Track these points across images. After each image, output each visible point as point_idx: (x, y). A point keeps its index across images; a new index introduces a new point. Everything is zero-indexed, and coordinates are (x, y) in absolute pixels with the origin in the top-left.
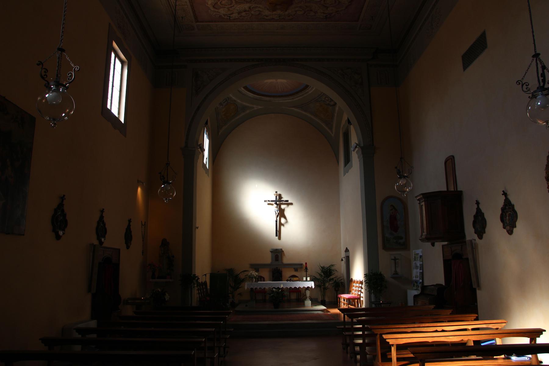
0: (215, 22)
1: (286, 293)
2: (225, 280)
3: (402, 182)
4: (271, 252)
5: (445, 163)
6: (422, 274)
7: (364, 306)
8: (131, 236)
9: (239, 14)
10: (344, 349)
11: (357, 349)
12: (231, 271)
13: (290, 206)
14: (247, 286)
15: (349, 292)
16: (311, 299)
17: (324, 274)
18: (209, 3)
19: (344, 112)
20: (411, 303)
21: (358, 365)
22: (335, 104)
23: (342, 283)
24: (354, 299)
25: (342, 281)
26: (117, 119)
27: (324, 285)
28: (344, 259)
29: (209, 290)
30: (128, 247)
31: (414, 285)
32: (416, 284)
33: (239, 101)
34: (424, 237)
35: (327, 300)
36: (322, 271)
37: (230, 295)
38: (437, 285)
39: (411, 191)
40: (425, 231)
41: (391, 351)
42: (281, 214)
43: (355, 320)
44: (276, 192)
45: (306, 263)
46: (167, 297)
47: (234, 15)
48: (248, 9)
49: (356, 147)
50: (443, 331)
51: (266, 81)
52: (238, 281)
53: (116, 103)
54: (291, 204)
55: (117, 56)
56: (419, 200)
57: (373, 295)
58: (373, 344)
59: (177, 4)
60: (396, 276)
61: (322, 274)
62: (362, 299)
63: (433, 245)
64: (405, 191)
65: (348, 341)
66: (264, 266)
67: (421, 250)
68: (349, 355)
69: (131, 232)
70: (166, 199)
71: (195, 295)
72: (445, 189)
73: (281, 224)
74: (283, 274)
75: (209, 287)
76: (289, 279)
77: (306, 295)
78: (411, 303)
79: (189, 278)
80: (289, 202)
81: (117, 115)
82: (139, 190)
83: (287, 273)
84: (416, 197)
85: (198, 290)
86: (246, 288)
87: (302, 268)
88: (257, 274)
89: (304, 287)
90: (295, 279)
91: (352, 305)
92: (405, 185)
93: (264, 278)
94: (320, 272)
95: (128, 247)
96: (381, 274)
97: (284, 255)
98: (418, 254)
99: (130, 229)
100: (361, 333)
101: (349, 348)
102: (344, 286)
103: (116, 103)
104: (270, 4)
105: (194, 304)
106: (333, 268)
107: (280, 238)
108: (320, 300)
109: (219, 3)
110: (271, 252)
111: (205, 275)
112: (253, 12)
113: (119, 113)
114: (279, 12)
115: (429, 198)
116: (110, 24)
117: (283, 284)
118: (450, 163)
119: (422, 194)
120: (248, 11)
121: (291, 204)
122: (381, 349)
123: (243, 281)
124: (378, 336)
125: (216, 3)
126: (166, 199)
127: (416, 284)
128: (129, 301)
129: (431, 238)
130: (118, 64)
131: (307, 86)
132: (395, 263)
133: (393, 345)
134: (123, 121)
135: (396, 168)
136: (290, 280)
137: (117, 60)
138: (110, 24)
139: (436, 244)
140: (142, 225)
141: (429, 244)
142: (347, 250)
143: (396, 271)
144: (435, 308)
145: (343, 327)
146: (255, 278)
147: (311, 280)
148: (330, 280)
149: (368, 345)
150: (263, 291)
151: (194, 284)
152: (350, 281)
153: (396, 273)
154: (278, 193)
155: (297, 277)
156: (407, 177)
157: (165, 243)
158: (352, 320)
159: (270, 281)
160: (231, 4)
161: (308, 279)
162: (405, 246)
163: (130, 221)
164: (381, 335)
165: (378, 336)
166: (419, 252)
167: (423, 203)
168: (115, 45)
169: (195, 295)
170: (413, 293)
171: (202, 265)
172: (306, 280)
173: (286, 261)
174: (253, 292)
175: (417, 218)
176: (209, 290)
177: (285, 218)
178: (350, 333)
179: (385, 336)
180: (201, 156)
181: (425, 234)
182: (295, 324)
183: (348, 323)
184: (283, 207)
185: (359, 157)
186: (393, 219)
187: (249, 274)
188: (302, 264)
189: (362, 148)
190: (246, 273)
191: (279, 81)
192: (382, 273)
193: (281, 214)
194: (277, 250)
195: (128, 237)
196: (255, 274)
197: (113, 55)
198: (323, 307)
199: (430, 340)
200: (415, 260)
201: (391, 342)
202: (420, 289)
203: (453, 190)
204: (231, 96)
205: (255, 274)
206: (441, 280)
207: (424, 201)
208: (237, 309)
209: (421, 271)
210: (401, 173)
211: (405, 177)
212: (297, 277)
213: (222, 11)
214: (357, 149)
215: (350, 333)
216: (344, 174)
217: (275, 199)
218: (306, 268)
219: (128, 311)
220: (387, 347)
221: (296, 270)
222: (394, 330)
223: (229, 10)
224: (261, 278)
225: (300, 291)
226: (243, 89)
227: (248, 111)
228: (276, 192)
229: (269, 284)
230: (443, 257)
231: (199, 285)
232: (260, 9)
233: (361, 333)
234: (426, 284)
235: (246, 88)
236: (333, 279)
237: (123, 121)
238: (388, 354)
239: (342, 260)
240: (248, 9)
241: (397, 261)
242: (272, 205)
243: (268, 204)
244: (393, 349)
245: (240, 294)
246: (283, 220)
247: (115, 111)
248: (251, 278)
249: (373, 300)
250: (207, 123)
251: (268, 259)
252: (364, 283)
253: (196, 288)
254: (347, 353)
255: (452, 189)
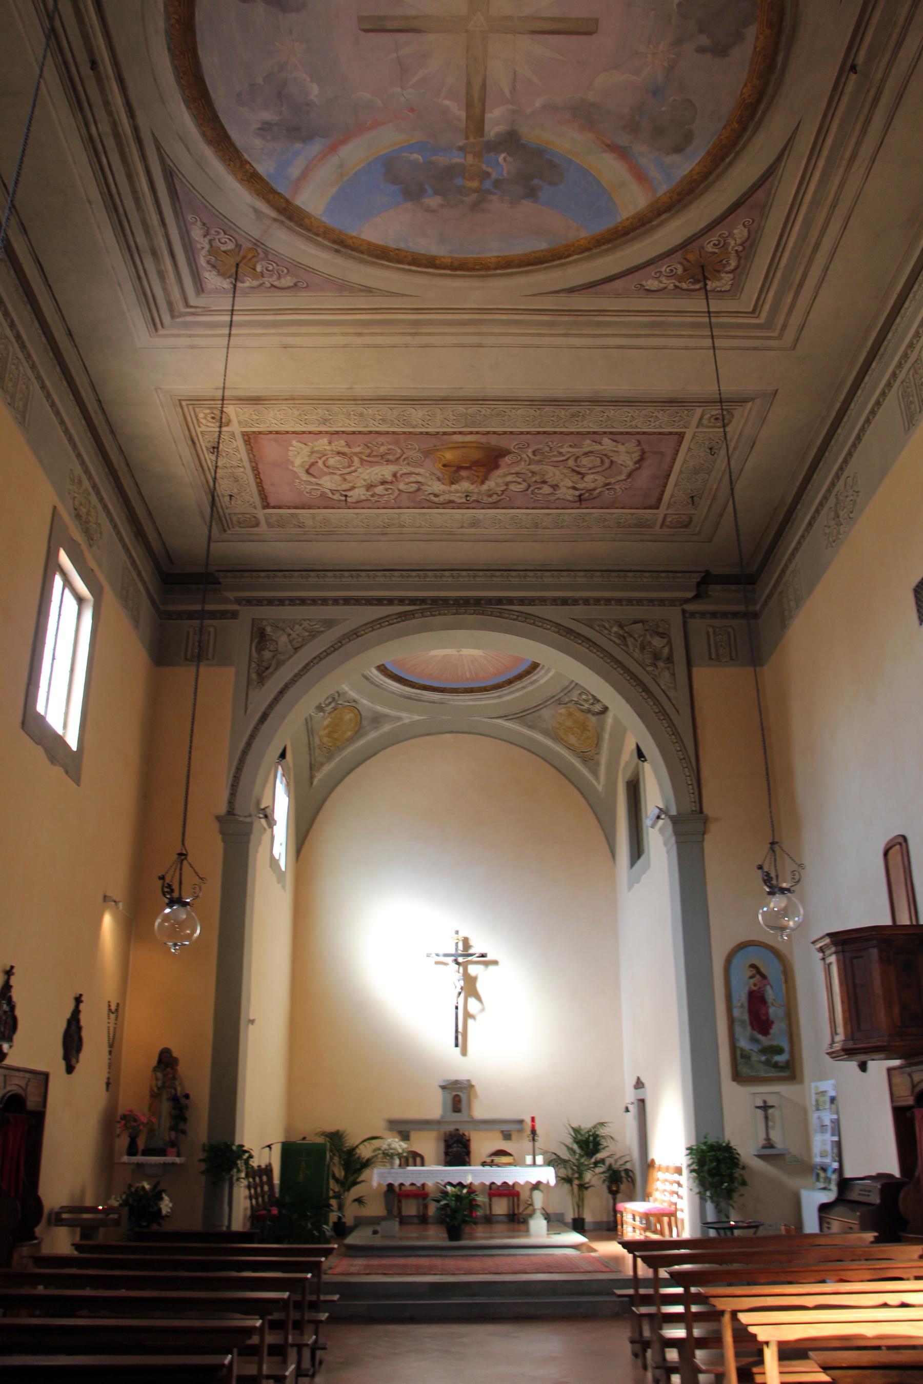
0: (309, 508)
1: (481, 1199)
2: (319, 1166)
3: (776, 903)
4: (443, 1088)
5: (886, 854)
6: (838, 1145)
7: (686, 1235)
8: (80, 1040)
9: (367, 490)
10: (636, 1355)
11: (672, 1355)
12: (336, 1137)
13: (492, 968)
14: (377, 1178)
15: (646, 1197)
16: (547, 1217)
17: (580, 1147)
18: (298, 462)
19: (627, 727)
20: (811, 1225)
21: (676, 1379)
22: (605, 709)
23: (627, 1171)
24: (659, 1216)
25: (628, 1166)
26: (60, 741)
27: (581, 1177)
28: (631, 1107)
29: (277, 1190)
30: (70, 1069)
31: (818, 1175)
32: (822, 1174)
33: (365, 702)
34: (837, 1047)
35: (588, 1217)
36: (578, 1142)
37: (333, 1202)
38: (880, 1176)
39: (799, 925)
40: (840, 1030)
41: (761, 1362)
42: (470, 987)
43: (663, 1273)
44: (457, 932)
45: (533, 1119)
46: (166, 1205)
47: (356, 491)
48: (389, 478)
49: (658, 817)
50: (904, 1305)
51: (434, 653)
52: (355, 1166)
53: (61, 702)
54: (495, 963)
55: (67, 583)
56: (821, 950)
57: (709, 1206)
58: (713, 1341)
59: (219, 464)
60: (769, 1153)
61: (575, 1147)
62: (679, 1215)
63: (863, 1067)
64: (783, 929)
65: (647, 1333)
66: (424, 1124)
67: (832, 1082)
68: (649, 1375)
69: (79, 1029)
70: (175, 945)
71: (241, 1202)
72: (888, 922)
73: (468, 1015)
74: (474, 1146)
75: (276, 1180)
76: (488, 1160)
77: (531, 1205)
78: (811, 1225)
79: (224, 1157)
80: (489, 958)
81: (60, 731)
82: (107, 921)
83: (482, 1145)
84: (813, 943)
85: (249, 1187)
86: (375, 1183)
87: (521, 1131)
88: (404, 1145)
89: (528, 1183)
90: (504, 1159)
91: (655, 1232)
92: (785, 912)
93: (422, 1158)
94: (569, 1141)
95: (70, 1069)
96: (728, 1149)
97: (476, 1096)
98: (824, 1093)
99: (78, 1021)
100: (680, 1309)
101: (649, 1353)
102: (633, 1181)
103: (61, 702)
104: (444, 466)
105: (239, 1223)
106: (602, 1131)
107: (464, 1053)
108: (569, 1216)
109: (320, 463)
110: (443, 1088)
111: (269, 1146)
112: (402, 486)
113: (65, 726)
114: (465, 485)
115: (847, 943)
116: (55, 508)
117: (472, 1175)
118: (897, 851)
119: (830, 935)
120: (391, 483)
121: (495, 963)
122: (737, 1355)
123: (367, 1164)
124: (727, 1318)
125: (313, 464)
126: (175, 945)
127: (822, 1174)
128: (64, 1216)
129: (857, 1049)
130: (70, 602)
131: (534, 666)
132: (766, 1118)
133: (767, 1343)
134: (74, 747)
135: (760, 867)
136: (492, 1164)
137: (67, 591)
138: (55, 508)
139: (871, 1065)
140: (110, 1010)
141: (851, 1066)
142: (639, 1084)
143: (768, 1139)
144: (877, 1240)
145: (631, 1291)
146: (400, 1156)
147: (549, 1163)
148: (596, 1164)
149: (701, 1343)
150: (420, 1194)
151: (239, 1171)
152: (648, 1166)
153: (769, 1145)
154: (462, 934)
155: (510, 1155)
156: (788, 890)
157: (166, 1061)
158: (656, 1272)
159: (438, 1164)
160: (349, 466)
161: (540, 1159)
162: (789, 1070)
163: (78, 1000)
164: (734, 1313)
165: (727, 1318)
166: (828, 1086)
167: (833, 959)
168: (64, 558)
169: (241, 1202)
170: (814, 1198)
171: (262, 1127)
172: (534, 1164)
173: (480, 1111)
174: (393, 1194)
175: (818, 999)
176: (277, 1190)
177: (478, 998)
178: (651, 1310)
179: (744, 1318)
180: (266, 837)
181: (840, 1037)
182: (504, 1283)
183: (646, 1282)
184: (473, 970)
185: (665, 844)
186: (756, 1000)
187: (385, 1146)
188: (521, 1122)
189: (676, 821)
190: (376, 1143)
191: (466, 652)
192: (732, 1145)
193: (470, 987)
194: (456, 1082)
195: (72, 1041)
196: (399, 1145)
197: (58, 581)
198: (576, 1238)
199: (869, 1331)
200: (818, 1109)
201: (762, 1334)
202: (834, 1187)
203: (907, 923)
204: (345, 687)
205: (399, 1145)
206: (892, 1167)
207: (836, 953)
208: (350, 1240)
209: (836, 1138)
210: (774, 882)
211: (783, 891)
212: (510, 1155)
213: (328, 483)
214: (661, 822)
215: (651, 1310)
216: (630, 887)
217: (453, 952)
218: (534, 1132)
219: (60, 1242)
220: (750, 1349)
221: (507, 1136)
222: (771, 1301)
223: (345, 480)
224: (414, 1158)
225: (517, 1194)
226: (375, 672)
227: (387, 728)
228: (457, 932)
229: (435, 1174)
230: (892, 1100)
231: (253, 1173)
232: (419, 479)
233: (680, 1309)
234: (849, 1173)
235: (382, 669)
236: (602, 1161)
237: (74, 747)
238: (755, 1370)
239: (627, 1110)
240: (389, 478)
241: (770, 1111)
242: (445, 964)
243: (437, 963)
244: (770, 1356)
245: (359, 1200)
246: (472, 1001)
247: (55, 721)
248: (388, 1155)
249: (657, 710)
250: (283, 755)
251: (434, 1107)
252: (685, 1171)
253: (244, 1183)
254: (645, 1367)
255: (904, 919)
